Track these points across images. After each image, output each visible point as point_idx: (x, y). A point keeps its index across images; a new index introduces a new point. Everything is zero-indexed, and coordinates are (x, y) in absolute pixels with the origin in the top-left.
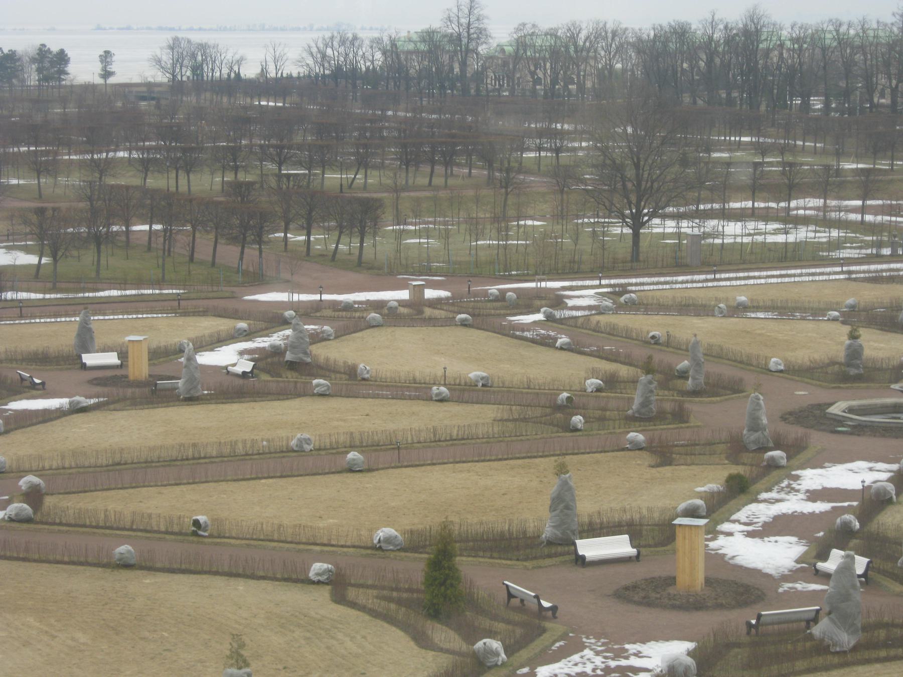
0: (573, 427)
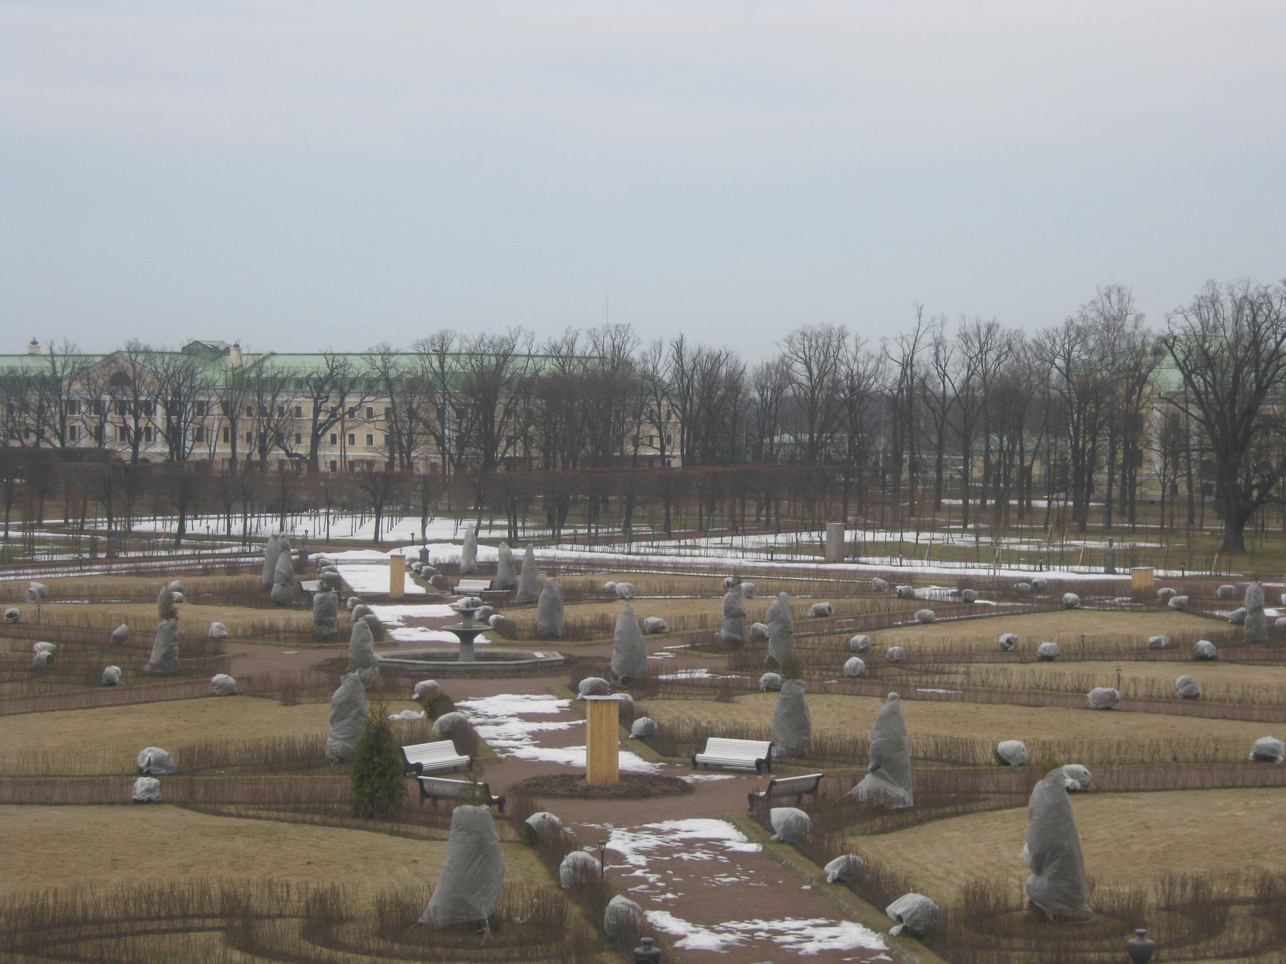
0: (108, 680)
